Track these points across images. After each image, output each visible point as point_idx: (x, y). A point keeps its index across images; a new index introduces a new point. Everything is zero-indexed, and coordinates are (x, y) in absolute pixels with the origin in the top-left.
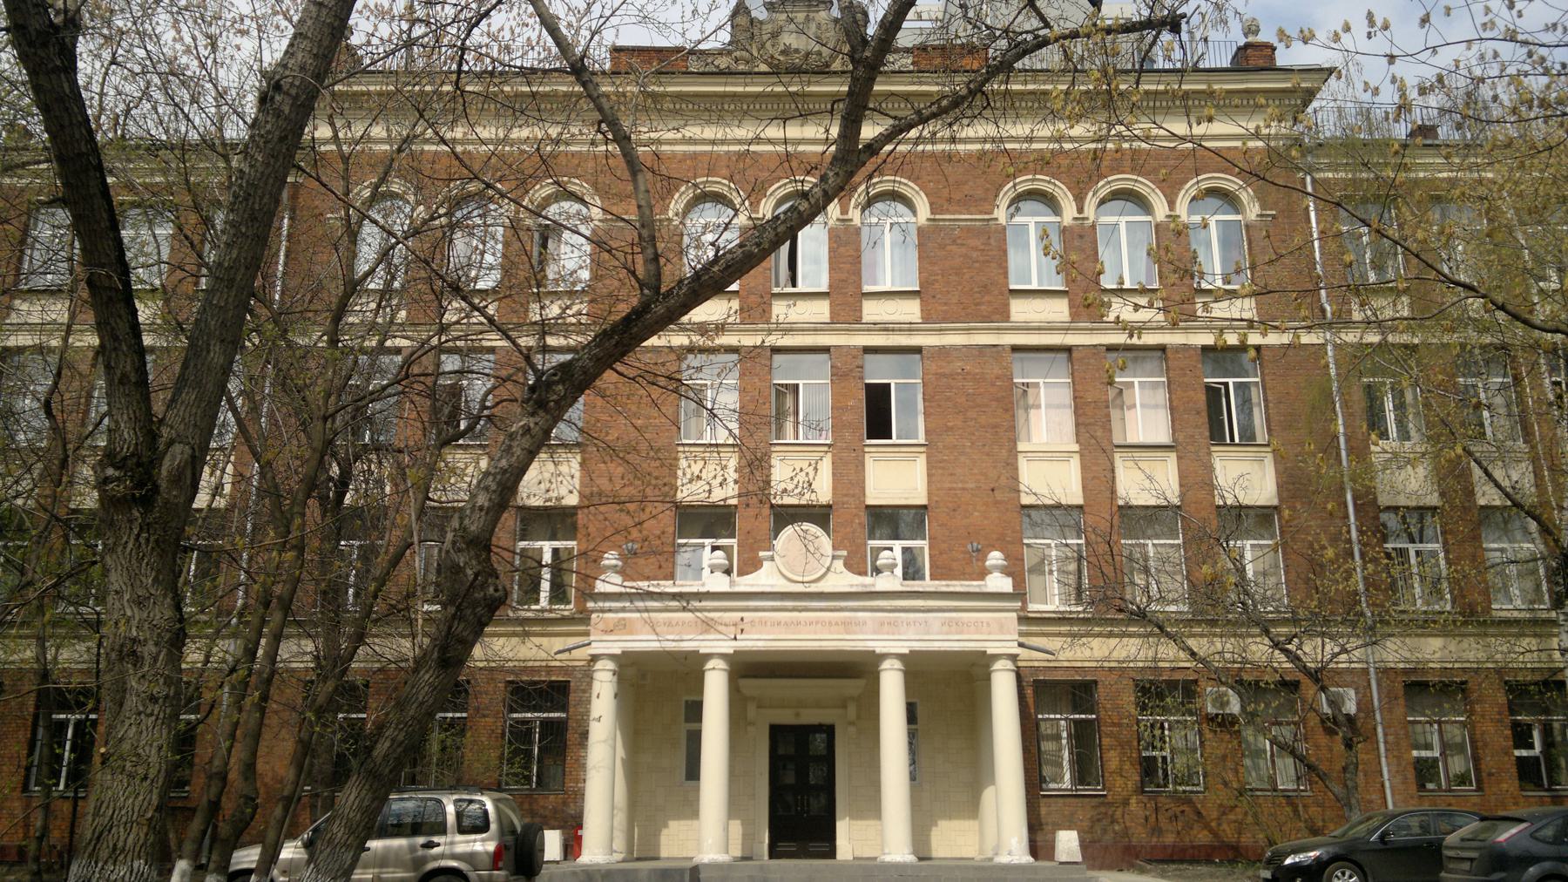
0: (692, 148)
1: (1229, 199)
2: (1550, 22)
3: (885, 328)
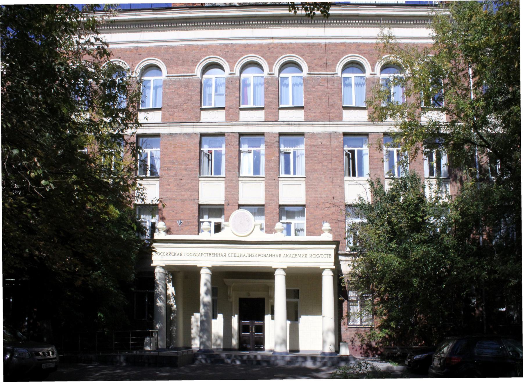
0: (136, 45)
3: (289, 124)
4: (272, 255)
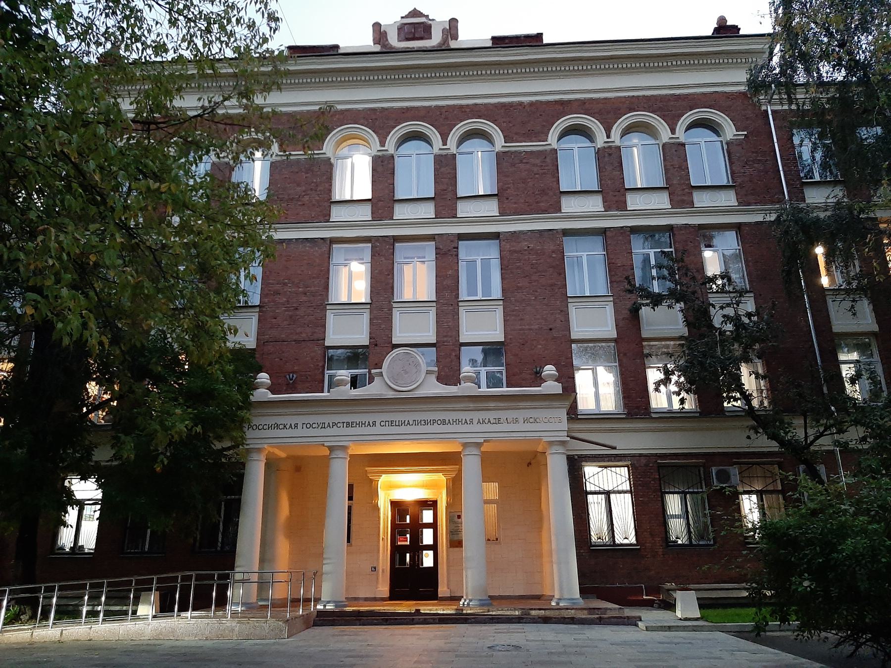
1: (712, 127)
2: (277, 32)
4: (458, 422)
